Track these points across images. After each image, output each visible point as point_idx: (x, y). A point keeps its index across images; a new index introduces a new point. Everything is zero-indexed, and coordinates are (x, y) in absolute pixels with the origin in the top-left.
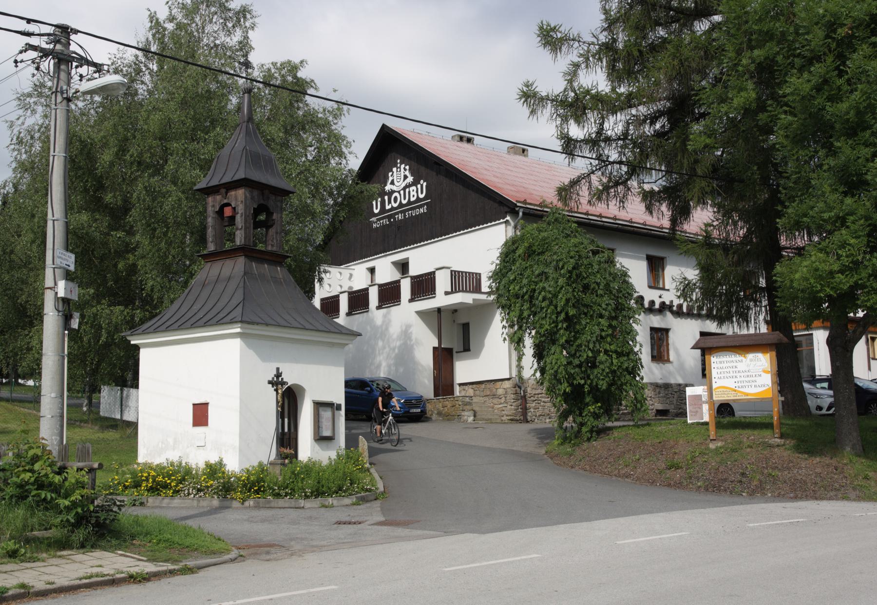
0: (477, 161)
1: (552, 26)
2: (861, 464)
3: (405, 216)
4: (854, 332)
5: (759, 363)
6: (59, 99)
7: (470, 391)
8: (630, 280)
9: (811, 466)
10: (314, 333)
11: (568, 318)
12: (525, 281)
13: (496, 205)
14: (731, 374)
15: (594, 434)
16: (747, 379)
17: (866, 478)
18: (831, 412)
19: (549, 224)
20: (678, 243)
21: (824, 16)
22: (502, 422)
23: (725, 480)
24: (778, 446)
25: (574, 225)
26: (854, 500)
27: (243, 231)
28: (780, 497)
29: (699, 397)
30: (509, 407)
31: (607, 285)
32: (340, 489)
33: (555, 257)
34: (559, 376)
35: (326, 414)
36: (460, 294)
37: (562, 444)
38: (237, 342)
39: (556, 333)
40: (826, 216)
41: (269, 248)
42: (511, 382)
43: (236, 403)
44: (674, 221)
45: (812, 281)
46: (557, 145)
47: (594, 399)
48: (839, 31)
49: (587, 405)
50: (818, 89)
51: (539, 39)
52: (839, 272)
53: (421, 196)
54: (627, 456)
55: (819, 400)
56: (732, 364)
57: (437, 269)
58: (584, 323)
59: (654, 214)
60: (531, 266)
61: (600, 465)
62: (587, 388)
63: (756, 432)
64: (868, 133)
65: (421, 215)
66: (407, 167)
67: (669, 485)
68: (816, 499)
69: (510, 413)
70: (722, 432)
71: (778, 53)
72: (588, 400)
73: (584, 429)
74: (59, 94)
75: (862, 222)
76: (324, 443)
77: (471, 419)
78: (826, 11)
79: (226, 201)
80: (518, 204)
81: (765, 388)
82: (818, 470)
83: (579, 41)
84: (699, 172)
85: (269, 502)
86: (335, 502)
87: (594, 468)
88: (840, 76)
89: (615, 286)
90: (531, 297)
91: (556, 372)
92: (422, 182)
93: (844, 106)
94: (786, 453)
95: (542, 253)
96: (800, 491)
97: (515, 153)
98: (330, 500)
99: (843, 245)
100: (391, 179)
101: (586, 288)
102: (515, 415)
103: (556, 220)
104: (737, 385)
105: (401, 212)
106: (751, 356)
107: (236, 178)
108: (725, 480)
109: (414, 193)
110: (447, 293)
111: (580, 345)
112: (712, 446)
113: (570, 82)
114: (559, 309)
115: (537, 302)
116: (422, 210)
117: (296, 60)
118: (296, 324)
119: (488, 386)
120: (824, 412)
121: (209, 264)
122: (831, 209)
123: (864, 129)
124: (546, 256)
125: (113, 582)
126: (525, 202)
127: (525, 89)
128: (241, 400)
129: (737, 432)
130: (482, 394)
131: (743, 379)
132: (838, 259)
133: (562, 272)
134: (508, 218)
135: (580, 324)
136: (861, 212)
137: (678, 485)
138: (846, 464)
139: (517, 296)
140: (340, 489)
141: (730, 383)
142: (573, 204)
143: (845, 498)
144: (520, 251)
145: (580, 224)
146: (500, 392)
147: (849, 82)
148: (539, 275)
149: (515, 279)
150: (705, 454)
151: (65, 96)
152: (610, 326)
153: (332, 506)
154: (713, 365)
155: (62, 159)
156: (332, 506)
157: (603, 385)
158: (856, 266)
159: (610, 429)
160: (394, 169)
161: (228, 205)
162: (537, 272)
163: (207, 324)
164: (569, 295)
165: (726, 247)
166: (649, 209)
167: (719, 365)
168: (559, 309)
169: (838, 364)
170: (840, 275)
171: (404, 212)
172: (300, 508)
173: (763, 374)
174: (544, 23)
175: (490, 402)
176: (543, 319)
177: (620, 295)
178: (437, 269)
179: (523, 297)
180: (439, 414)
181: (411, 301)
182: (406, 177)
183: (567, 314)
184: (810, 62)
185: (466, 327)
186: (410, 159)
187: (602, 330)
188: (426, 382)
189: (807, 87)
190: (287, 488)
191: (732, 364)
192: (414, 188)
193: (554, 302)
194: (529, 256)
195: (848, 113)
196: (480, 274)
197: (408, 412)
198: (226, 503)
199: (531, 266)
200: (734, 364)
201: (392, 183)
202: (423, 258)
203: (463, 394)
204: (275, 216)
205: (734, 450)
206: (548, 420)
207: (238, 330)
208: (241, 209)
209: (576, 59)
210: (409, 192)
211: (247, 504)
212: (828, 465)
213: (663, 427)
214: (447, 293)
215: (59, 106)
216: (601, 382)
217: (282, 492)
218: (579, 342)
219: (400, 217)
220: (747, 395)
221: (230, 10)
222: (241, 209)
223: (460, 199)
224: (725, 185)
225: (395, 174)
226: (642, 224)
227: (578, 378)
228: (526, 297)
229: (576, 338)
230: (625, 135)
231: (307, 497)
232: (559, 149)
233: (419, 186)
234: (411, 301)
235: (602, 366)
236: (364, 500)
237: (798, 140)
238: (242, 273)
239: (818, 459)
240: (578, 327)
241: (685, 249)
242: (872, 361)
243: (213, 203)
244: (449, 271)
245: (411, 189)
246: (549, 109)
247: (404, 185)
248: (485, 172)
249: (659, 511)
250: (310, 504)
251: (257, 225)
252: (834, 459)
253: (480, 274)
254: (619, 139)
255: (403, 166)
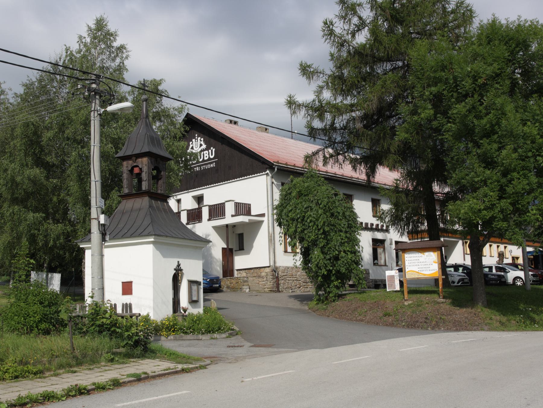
0: (244, 137)
1: (308, 64)
2: (487, 312)
3: (201, 168)
4: (483, 240)
5: (431, 258)
6: (96, 114)
7: (244, 274)
8: (355, 211)
9: (462, 313)
10: (189, 241)
11: (324, 233)
12: (298, 211)
13: (260, 164)
14: (416, 264)
15: (337, 298)
16: (425, 266)
17: (491, 319)
18: (459, 284)
19: (308, 178)
20: (379, 190)
21: (471, 72)
22: (265, 292)
23: (417, 321)
24: (442, 303)
25: (322, 179)
26: (487, 331)
27: (147, 182)
28: (448, 330)
29: (393, 277)
30: (269, 283)
31: (344, 213)
32: (219, 329)
33: (316, 198)
34: (319, 265)
35: (195, 287)
36: (242, 216)
37: (317, 304)
38: (151, 246)
39: (317, 241)
40: (476, 180)
41: (159, 192)
42: (270, 268)
43: (151, 282)
44: (368, 175)
45: (470, 214)
46: (305, 131)
47: (334, 278)
48: (479, 80)
49: (333, 281)
50: (469, 111)
51: (300, 71)
52: (483, 210)
53: (212, 157)
54: (359, 310)
55: (453, 278)
56: (416, 258)
57: (226, 202)
58: (332, 235)
59: (358, 170)
60: (301, 203)
61: (344, 315)
62: (334, 272)
63: (429, 295)
64: (496, 136)
65: (211, 168)
66: (202, 139)
67: (387, 325)
68: (468, 330)
69: (269, 287)
70: (411, 296)
71: (444, 90)
72: (333, 278)
73: (331, 295)
74: (96, 112)
75: (496, 183)
76: (193, 304)
77: (248, 290)
78: (472, 69)
79: (135, 164)
80: (275, 164)
81: (433, 272)
82: (466, 315)
83: (323, 74)
84: (392, 150)
85: (182, 337)
86: (218, 336)
87: (341, 316)
88: (481, 105)
89: (347, 213)
90: (303, 220)
91: (318, 263)
92: (212, 148)
93: (484, 121)
94: (448, 307)
95: (307, 195)
96: (459, 326)
97: (262, 131)
98: (215, 335)
99: (486, 196)
100: (191, 146)
101: (332, 215)
102: (273, 288)
103: (312, 176)
104: (419, 269)
105: (198, 166)
106: (427, 254)
107: (143, 151)
108: (417, 321)
109: (206, 155)
110: (232, 216)
111: (330, 248)
112: (406, 303)
113: (318, 96)
114: (319, 227)
115: (306, 223)
116: (212, 165)
117: (158, 79)
118: (180, 236)
119: (255, 271)
120: (456, 284)
121: (125, 201)
122: (478, 176)
123: (494, 134)
124: (311, 197)
125: (176, 372)
126: (278, 162)
127: (289, 99)
128: (154, 280)
129: (418, 295)
130: (252, 275)
131: (422, 266)
132: (484, 203)
133: (321, 206)
134: (268, 171)
135: (330, 235)
136: (495, 178)
137: (392, 325)
138: (480, 312)
139: (293, 220)
140: (219, 329)
141: (416, 269)
142: (314, 166)
143: (482, 330)
144: (294, 194)
145: (326, 179)
146: (263, 274)
147: (486, 108)
148: (306, 208)
149: (291, 210)
150: (403, 308)
151: (99, 113)
152: (346, 237)
153: (216, 339)
154: (406, 259)
155: (99, 147)
156: (216, 339)
157: (343, 270)
158: (492, 207)
159: (345, 295)
160: (194, 140)
161: (137, 166)
162: (305, 206)
163: (132, 236)
164: (325, 220)
165: (407, 192)
166: (354, 168)
167: (410, 259)
168: (319, 227)
169: (475, 258)
170: (485, 211)
171: (200, 166)
172: (214, 339)
173: (434, 264)
174: (303, 62)
175: (256, 280)
176: (310, 232)
177: (350, 219)
178: (226, 202)
179: (297, 220)
180: (228, 287)
181: (209, 220)
182: (201, 145)
183: (324, 230)
184: (466, 96)
185: (241, 237)
186: (204, 134)
187: (342, 239)
188: (218, 268)
189: (464, 110)
190: (190, 328)
191: (416, 258)
192: (207, 152)
193: (316, 223)
194: (299, 197)
195: (486, 125)
196: (250, 205)
197: (212, 286)
198: (157, 338)
199: (301, 203)
200: (418, 258)
201: (192, 148)
202: (213, 194)
203: (239, 276)
204: (162, 173)
205: (419, 306)
206: (290, 291)
207: (152, 240)
208: (145, 169)
209: (321, 84)
210: (204, 154)
211: (169, 338)
212: (471, 313)
213: (373, 293)
214: (232, 216)
215: (96, 118)
216: (342, 269)
217: (188, 331)
218: (330, 245)
219: (198, 169)
220: (425, 275)
221: (113, 47)
222: (145, 169)
223: (237, 160)
224: (404, 156)
225: (194, 143)
226: (302, 168)
227: (329, 266)
228: (299, 220)
229: (328, 244)
230: (345, 128)
231: (203, 334)
232: (307, 134)
233: (210, 151)
234: (209, 220)
235: (343, 260)
236: (231, 335)
237: (458, 137)
238: (148, 207)
239: (465, 309)
240: (329, 237)
241: (384, 193)
242: (466, 255)
243: (126, 166)
244: (233, 203)
245: (205, 152)
246: (303, 111)
247: (200, 150)
248: (250, 143)
249: (402, 337)
250: (204, 337)
251: (154, 178)
252: (473, 309)
253: (250, 205)
254: (342, 129)
255: (199, 138)
